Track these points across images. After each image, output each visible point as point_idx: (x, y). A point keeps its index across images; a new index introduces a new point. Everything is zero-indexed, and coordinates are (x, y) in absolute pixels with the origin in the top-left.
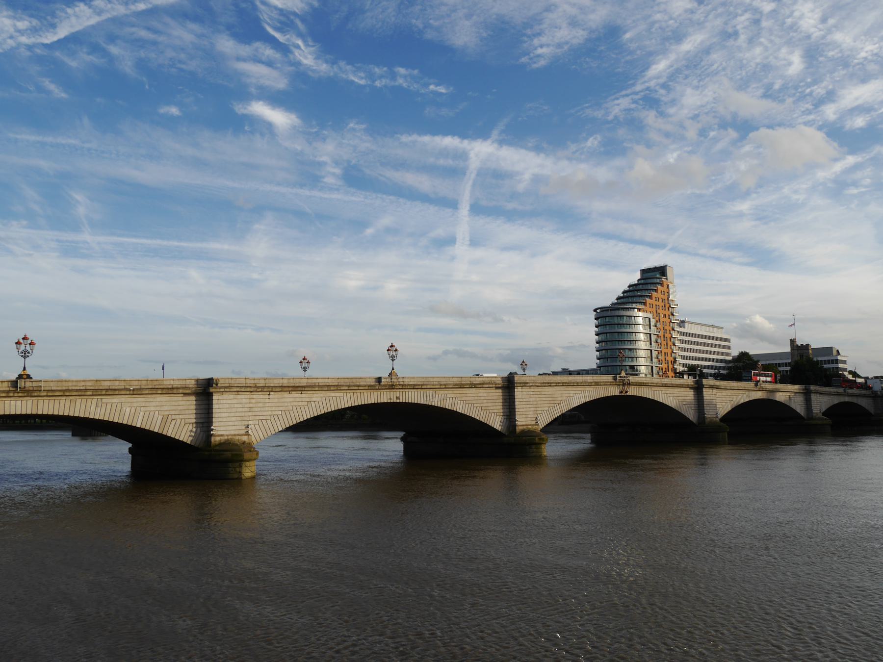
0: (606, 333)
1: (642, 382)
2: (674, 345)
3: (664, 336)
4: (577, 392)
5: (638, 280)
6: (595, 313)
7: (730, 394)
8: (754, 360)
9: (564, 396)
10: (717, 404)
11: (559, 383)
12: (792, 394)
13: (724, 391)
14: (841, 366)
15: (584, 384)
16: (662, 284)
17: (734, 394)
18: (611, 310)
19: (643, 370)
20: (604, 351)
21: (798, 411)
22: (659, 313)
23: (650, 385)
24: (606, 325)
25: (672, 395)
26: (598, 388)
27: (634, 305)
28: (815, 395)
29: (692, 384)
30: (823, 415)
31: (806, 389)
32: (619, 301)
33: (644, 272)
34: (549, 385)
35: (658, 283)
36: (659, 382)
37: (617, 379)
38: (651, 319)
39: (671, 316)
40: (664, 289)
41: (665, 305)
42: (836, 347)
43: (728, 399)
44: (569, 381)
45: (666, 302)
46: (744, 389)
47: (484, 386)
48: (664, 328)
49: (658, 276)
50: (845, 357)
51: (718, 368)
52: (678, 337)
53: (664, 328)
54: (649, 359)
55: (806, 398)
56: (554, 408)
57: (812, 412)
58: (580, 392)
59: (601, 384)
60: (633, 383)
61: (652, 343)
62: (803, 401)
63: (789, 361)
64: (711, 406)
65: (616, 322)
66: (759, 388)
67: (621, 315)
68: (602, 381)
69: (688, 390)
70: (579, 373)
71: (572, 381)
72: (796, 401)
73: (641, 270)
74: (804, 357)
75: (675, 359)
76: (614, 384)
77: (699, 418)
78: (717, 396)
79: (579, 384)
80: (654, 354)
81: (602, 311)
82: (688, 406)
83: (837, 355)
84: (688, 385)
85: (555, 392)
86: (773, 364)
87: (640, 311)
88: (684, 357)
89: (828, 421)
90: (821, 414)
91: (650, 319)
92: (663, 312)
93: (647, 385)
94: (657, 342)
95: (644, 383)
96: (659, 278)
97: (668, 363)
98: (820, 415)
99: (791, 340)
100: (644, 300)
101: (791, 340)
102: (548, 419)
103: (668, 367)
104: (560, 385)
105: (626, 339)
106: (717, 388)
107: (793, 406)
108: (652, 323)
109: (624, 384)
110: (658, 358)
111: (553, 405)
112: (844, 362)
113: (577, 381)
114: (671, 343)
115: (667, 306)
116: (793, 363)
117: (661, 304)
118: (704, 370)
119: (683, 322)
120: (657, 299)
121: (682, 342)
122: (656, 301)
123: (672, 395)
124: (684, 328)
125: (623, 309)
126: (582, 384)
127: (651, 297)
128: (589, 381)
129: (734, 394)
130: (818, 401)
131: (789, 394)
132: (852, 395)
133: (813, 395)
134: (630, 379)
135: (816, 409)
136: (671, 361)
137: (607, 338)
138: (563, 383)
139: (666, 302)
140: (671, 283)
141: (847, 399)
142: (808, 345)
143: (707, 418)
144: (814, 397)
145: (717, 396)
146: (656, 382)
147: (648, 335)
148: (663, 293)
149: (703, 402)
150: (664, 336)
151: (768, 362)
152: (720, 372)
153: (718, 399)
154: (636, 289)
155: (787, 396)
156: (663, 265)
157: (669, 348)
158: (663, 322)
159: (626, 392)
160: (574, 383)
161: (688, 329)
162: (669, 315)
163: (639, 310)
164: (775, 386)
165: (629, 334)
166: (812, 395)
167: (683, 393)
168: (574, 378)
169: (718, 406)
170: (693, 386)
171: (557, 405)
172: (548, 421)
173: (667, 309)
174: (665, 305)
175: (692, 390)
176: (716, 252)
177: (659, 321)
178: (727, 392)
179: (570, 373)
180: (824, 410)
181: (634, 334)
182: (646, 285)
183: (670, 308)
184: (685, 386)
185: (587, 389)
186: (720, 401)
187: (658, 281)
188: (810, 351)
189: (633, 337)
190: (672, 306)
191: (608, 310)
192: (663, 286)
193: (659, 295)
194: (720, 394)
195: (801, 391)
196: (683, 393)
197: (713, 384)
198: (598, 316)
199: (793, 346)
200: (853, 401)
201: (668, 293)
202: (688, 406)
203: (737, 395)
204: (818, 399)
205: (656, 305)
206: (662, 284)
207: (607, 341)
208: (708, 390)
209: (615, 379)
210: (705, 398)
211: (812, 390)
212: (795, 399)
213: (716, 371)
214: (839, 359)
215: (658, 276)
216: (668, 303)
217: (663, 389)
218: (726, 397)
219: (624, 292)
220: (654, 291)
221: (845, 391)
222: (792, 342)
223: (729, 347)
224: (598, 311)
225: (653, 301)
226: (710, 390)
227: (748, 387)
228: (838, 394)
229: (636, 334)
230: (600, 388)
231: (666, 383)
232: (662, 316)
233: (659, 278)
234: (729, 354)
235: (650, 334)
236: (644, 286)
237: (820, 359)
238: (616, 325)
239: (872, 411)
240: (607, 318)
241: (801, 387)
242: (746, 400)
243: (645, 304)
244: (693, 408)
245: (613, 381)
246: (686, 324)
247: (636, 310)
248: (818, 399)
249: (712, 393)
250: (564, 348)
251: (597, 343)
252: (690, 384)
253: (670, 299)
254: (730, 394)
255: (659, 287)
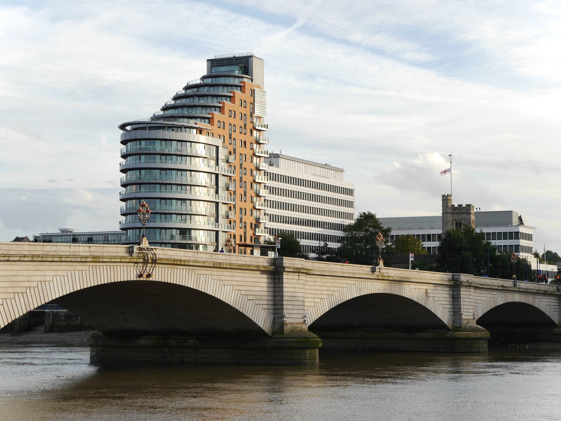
0: (140, 169)
1: (179, 258)
2: (258, 195)
3: (241, 178)
4: (60, 273)
5: (203, 78)
6: (122, 132)
7: (329, 284)
8: (382, 227)
9: (34, 279)
10: (306, 300)
11: (25, 256)
12: (431, 288)
13: (319, 279)
14: (523, 242)
15: (73, 260)
16: (242, 88)
17: (335, 285)
18: (150, 128)
19: (201, 237)
20: (134, 201)
21: (439, 314)
22: (234, 139)
23: (191, 264)
24: (140, 154)
25: (230, 283)
26: (98, 267)
27: (191, 120)
28: (467, 290)
29: (266, 264)
30: (477, 324)
31: (454, 279)
32: (166, 112)
33: (214, 63)
34: (7, 258)
35: (236, 86)
36: (208, 260)
37: (133, 252)
38: (220, 149)
39: (255, 145)
40: (246, 96)
41: (245, 125)
42: (518, 211)
43: (324, 292)
44: (45, 253)
45: (249, 119)
46: (351, 276)
47: (11, 259)
48: (241, 165)
49: (237, 73)
50: (530, 228)
51: (325, 238)
52: (266, 182)
53: (241, 165)
54: (213, 219)
55: (453, 295)
56: (13, 300)
57: (461, 318)
58: (65, 273)
59: (104, 260)
60: (161, 259)
61: (220, 190)
62: (449, 299)
63: (440, 231)
64: (296, 303)
65: (158, 150)
66: (378, 276)
67: (168, 138)
68: (105, 254)
69: (258, 274)
70: (90, 239)
71: (51, 253)
72: (436, 299)
73: (208, 60)
74: (462, 227)
75: (258, 220)
76: (128, 260)
77: (274, 323)
78: (307, 287)
79: (63, 259)
80: (223, 209)
81: (134, 129)
82: (257, 302)
83: (518, 225)
84: (258, 266)
85: (18, 273)
86: (414, 235)
87: (201, 133)
88: (273, 218)
89: (485, 333)
90: (475, 322)
91: (217, 147)
92: (243, 137)
93: (186, 263)
94: (227, 189)
95: (180, 261)
96: (239, 77)
97: (245, 227)
98: (474, 324)
99: (443, 196)
100: (209, 114)
101: (443, 196)
102: (315, 316)
103: (245, 233)
104: (27, 259)
105: (174, 182)
106: (306, 274)
107: (430, 306)
108: (222, 156)
109: (146, 262)
110: (228, 217)
111: (12, 296)
112: (529, 237)
113: (61, 254)
114: (252, 191)
115: (249, 126)
116: (443, 236)
117: (238, 122)
118: (302, 240)
119: (277, 156)
120: (232, 114)
121: (272, 190)
122: (230, 117)
123: (230, 283)
124: (278, 166)
125: (172, 127)
126: (70, 259)
127: (221, 109)
128: (82, 254)
129: (335, 285)
130: (472, 300)
131: (426, 287)
132: (526, 292)
133: (464, 289)
134: (157, 252)
135: (467, 314)
136: (251, 224)
137: (140, 178)
138: (33, 256)
139: (249, 119)
140: (260, 88)
141: (517, 298)
142: (469, 206)
143: (287, 324)
144: (464, 293)
145: (307, 287)
146: (202, 260)
147: (214, 176)
148: (243, 103)
149: (282, 296)
150: (241, 178)
151: (405, 233)
152: (327, 245)
153: (308, 291)
154: (198, 93)
155: (422, 291)
156: (246, 55)
157: (249, 200)
158: (241, 154)
159: (149, 276)
160: (53, 256)
161: (283, 169)
162: (251, 143)
163: (200, 131)
164: (404, 272)
165: (179, 172)
166: (462, 289)
167: (249, 279)
168: (54, 248)
169: (306, 304)
170: (266, 269)
171: (21, 295)
172: (317, 315)
173: (249, 133)
174: (245, 125)
175: (265, 276)
176: (378, 40)
177: (235, 152)
178: (325, 280)
179: (75, 239)
180: (480, 315)
181: (188, 173)
182: (216, 88)
183: (255, 132)
184: (252, 268)
185: (78, 268)
186: (311, 296)
187: (236, 82)
188: (473, 217)
189: (187, 178)
190: (257, 128)
191: (144, 128)
192: (244, 92)
193: (236, 107)
194: (312, 283)
195: (445, 283)
196: (249, 279)
197: (300, 266)
198: (128, 138)
199: (447, 206)
200: (527, 302)
201: (253, 104)
202: (257, 302)
203: (340, 285)
204: (471, 297)
205: (230, 124)
206: (242, 88)
207: (140, 184)
208: (291, 276)
209: (131, 252)
210: (285, 289)
211: (462, 282)
212: (436, 295)
213: (321, 242)
214: (520, 231)
215: (237, 73)
216: (252, 122)
217: (215, 272)
218: (322, 288)
219: (177, 98)
220: (228, 99)
221: (515, 286)
222: (446, 199)
223: (350, 204)
224: (128, 128)
225: (225, 118)
226: (296, 276)
227: (359, 274)
228: (504, 289)
229: (193, 173)
230: (122, 267)
231: (219, 261)
232: (238, 143)
233: (239, 77)
234: (350, 216)
235: (217, 175)
236: (212, 88)
237: (486, 230)
238: (158, 156)
239: (555, 318)
240: (143, 142)
241: (446, 276)
242: (355, 294)
243: (210, 120)
244: (265, 307)
245: (127, 255)
246: (281, 160)
247: (195, 130)
248: (471, 297)
249: (297, 282)
250: (96, 191)
251: (124, 185)
252: (262, 264)
253: (254, 115)
254: (329, 284)
255: (238, 92)
